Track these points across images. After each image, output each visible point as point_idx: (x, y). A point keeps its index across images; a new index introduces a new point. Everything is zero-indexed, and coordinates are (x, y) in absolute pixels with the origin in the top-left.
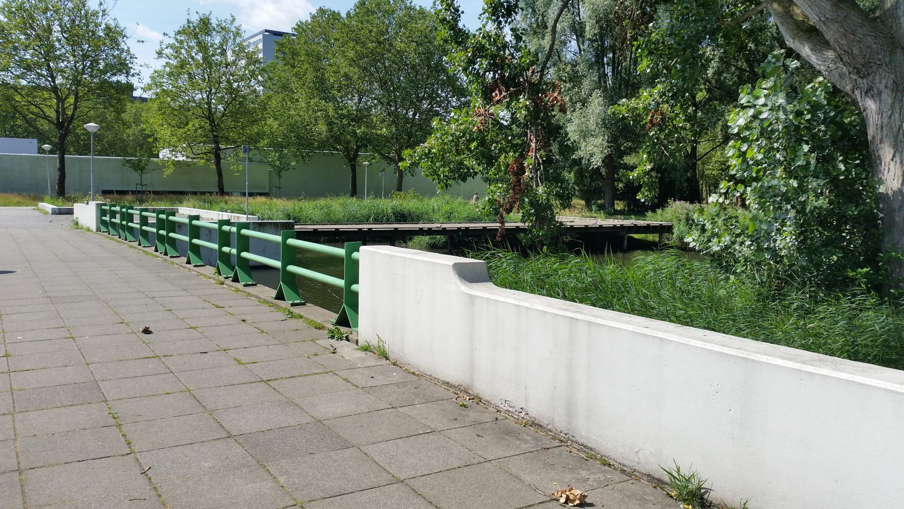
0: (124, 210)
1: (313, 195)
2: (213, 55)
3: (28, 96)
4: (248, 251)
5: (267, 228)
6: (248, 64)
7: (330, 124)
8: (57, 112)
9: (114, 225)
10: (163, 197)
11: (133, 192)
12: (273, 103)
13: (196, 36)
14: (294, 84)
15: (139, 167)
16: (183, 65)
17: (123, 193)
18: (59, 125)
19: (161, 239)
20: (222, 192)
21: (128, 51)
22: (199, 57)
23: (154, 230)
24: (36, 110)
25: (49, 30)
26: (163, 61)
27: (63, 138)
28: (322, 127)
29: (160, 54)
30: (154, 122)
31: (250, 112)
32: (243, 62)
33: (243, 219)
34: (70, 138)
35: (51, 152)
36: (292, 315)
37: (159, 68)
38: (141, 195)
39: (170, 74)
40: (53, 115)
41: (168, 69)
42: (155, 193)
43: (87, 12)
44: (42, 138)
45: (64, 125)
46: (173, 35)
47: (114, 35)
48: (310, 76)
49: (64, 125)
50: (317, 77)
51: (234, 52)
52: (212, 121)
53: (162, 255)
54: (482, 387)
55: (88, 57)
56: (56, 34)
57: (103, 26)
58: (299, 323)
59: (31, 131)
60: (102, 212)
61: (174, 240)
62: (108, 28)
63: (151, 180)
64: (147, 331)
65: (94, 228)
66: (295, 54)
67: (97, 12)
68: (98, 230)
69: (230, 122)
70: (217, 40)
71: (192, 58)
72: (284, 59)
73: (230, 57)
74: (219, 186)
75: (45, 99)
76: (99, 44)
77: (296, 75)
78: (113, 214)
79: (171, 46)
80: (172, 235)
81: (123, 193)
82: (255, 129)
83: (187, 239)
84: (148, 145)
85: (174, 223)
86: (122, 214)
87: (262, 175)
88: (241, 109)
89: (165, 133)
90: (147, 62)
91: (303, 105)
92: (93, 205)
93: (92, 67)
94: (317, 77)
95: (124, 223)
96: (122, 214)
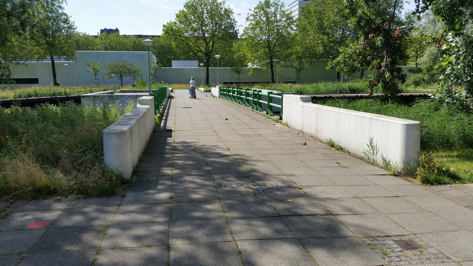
0: (239, 90)
1: (311, 81)
2: (271, 18)
3: (195, 42)
4: (272, 103)
5: (359, 103)
6: (287, 20)
7: (325, 46)
8: (206, 49)
9: (234, 97)
10: (246, 85)
11: (236, 83)
12: (298, 38)
13: (263, 9)
14: (309, 28)
15: (238, 72)
16: (258, 23)
17: (231, 83)
18: (207, 55)
19: (255, 103)
20: (274, 82)
21: (234, 20)
22: (264, 19)
23: (245, 97)
24: (198, 49)
25: (203, 13)
26: (249, 22)
27: (208, 60)
28: (321, 48)
29: (247, 19)
30: (245, 51)
31: (286, 43)
32: (284, 19)
33: (276, 92)
34: (211, 59)
35: (204, 66)
36: (269, 118)
37: (247, 26)
38: (239, 84)
39: (252, 28)
40: (204, 50)
41: (251, 26)
42: (245, 83)
43: (217, 3)
44: (200, 60)
45: (208, 54)
46: (253, 10)
47: (228, 13)
48: (316, 23)
49: (208, 54)
50: (319, 24)
51: (280, 15)
52: (269, 49)
53: (255, 110)
54: (305, 130)
55: (218, 24)
56: (205, 15)
57: (224, 9)
58: (271, 119)
59: (195, 57)
60: (221, 90)
61: (261, 103)
62: (226, 10)
63: (244, 78)
64: (226, 119)
65: (218, 96)
66: (309, 12)
67: (221, 3)
68: (219, 97)
69: (277, 49)
70: (273, 10)
71: (262, 20)
72: (304, 15)
73: (278, 17)
74: (272, 79)
75: (201, 44)
76: (222, 17)
77: (309, 23)
78: (234, 92)
79: (253, 15)
80: (260, 101)
81: (231, 83)
82: (289, 51)
83: (252, 99)
84: (242, 62)
85: (261, 95)
86: (238, 91)
87: (292, 73)
88: (284, 42)
89: (249, 55)
90: (242, 25)
91: (312, 37)
92: (217, 87)
93: (219, 28)
94: (319, 24)
95: (239, 96)
96: (238, 91)
